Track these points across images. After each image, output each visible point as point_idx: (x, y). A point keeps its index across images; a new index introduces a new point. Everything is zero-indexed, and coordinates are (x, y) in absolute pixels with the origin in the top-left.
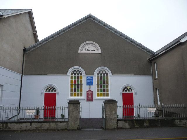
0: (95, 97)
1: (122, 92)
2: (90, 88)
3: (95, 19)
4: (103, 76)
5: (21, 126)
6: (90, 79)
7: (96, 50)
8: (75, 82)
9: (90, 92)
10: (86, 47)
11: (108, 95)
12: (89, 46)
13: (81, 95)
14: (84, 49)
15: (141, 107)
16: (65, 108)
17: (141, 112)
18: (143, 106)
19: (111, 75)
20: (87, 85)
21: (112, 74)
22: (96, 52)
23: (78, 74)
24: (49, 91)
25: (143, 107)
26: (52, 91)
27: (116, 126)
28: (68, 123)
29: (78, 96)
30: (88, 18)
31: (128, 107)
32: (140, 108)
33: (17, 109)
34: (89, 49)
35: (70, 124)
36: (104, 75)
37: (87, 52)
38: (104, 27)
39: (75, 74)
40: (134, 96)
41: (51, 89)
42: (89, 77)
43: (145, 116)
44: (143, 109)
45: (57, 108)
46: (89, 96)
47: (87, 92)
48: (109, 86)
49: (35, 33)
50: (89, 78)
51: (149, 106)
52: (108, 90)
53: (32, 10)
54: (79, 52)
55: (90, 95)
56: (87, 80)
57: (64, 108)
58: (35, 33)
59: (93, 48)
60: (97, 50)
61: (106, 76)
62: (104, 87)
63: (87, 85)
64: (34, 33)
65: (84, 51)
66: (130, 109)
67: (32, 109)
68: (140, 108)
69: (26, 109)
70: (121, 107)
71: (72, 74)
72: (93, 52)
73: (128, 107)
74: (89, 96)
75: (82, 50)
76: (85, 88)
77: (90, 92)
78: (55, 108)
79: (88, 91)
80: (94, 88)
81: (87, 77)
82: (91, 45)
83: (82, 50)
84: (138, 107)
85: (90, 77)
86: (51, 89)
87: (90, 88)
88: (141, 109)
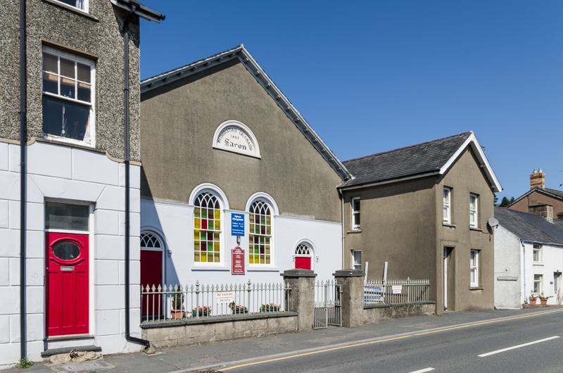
0: (248, 265)
5: (215, 331)
6: (238, 220)
7: (248, 148)
8: (204, 225)
10: (229, 134)
14: (223, 139)
15: (200, 290)
17: (238, 299)
18: (205, 286)
19: (277, 214)
20: (233, 234)
21: (280, 214)
28: (298, 319)
29: (210, 260)
32: (249, 291)
34: (234, 141)
35: (301, 319)
37: (229, 148)
42: (237, 215)
43: (224, 313)
46: (237, 262)
47: (234, 251)
48: (271, 241)
50: (238, 219)
51: (220, 286)
52: (268, 248)
54: (215, 145)
56: (233, 221)
59: (242, 140)
61: (266, 215)
62: (262, 241)
63: (233, 234)
65: (222, 145)
66: (157, 295)
67: (227, 291)
68: (249, 291)
69: (215, 289)
74: (237, 262)
76: (226, 242)
77: (238, 252)
80: (245, 243)
81: (233, 215)
82: (238, 131)
85: (239, 215)
87: (238, 243)
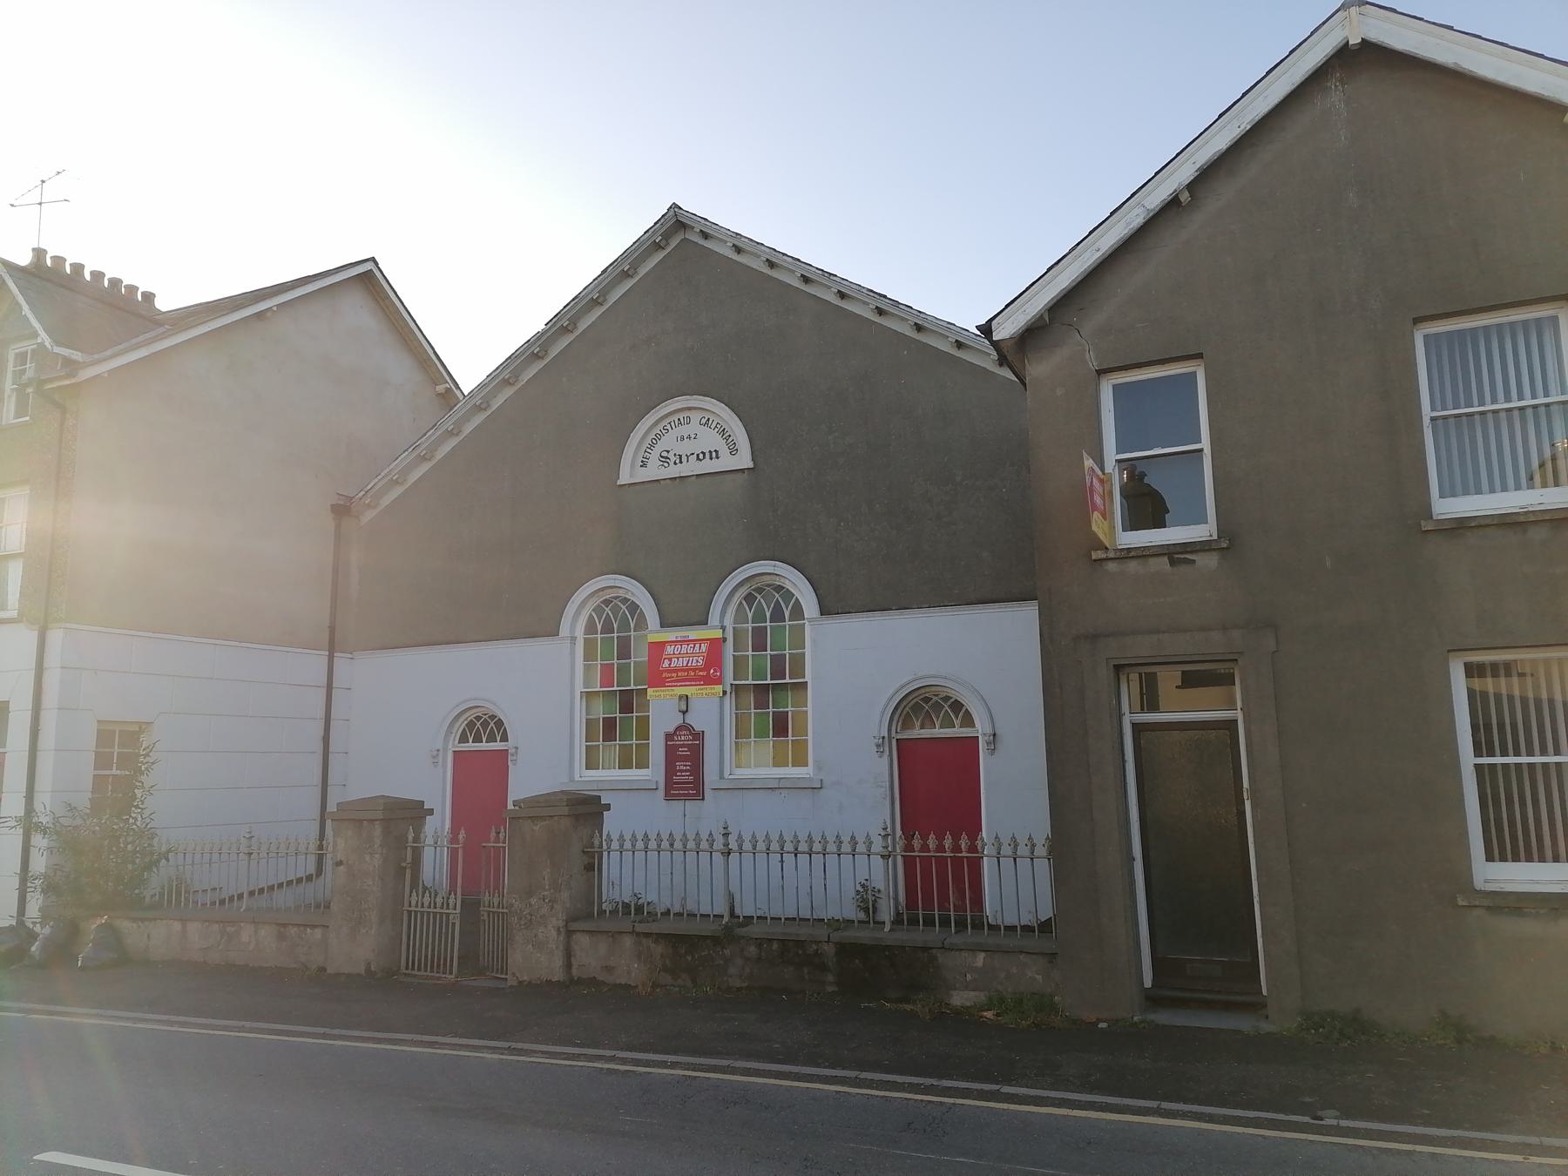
1: (454, 745)
2: (684, 713)
3: (708, 231)
4: (768, 623)
9: (684, 738)
11: (800, 761)
12: (684, 430)
13: (643, 764)
16: (685, 841)
22: (727, 462)
23: (624, 626)
24: (478, 739)
25: (747, 846)
26: (491, 739)
27: (558, 962)
30: (667, 236)
31: (941, 848)
33: (877, 846)
34: (685, 448)
36: (778, 615)
37: (673, 471)
38: (774, 274)
39: (608, 628)
40: (985, 763)
41: (485, 724)
44: (747, 857)
45: (430, 841)
46: (680, 765)
49: (449, 390)
53: (373, 260)
54: (624, 479)
55: (685, 759)
57: (761, 846)
58: (449, 390)
60: (734, 451)
64: (441, 388)
65: (654, 471)
70: (1041, 850)
71: (590, 628)
72: (708, 466)
73: (941, 848)
74: (680, 765)
75: (644, 465)
78: (973, 848)
79: (672, 730)
83: (644, 465)
84: (719, 844)
86: (485, 724)
87: (684, 713)
88: (734, 857)
